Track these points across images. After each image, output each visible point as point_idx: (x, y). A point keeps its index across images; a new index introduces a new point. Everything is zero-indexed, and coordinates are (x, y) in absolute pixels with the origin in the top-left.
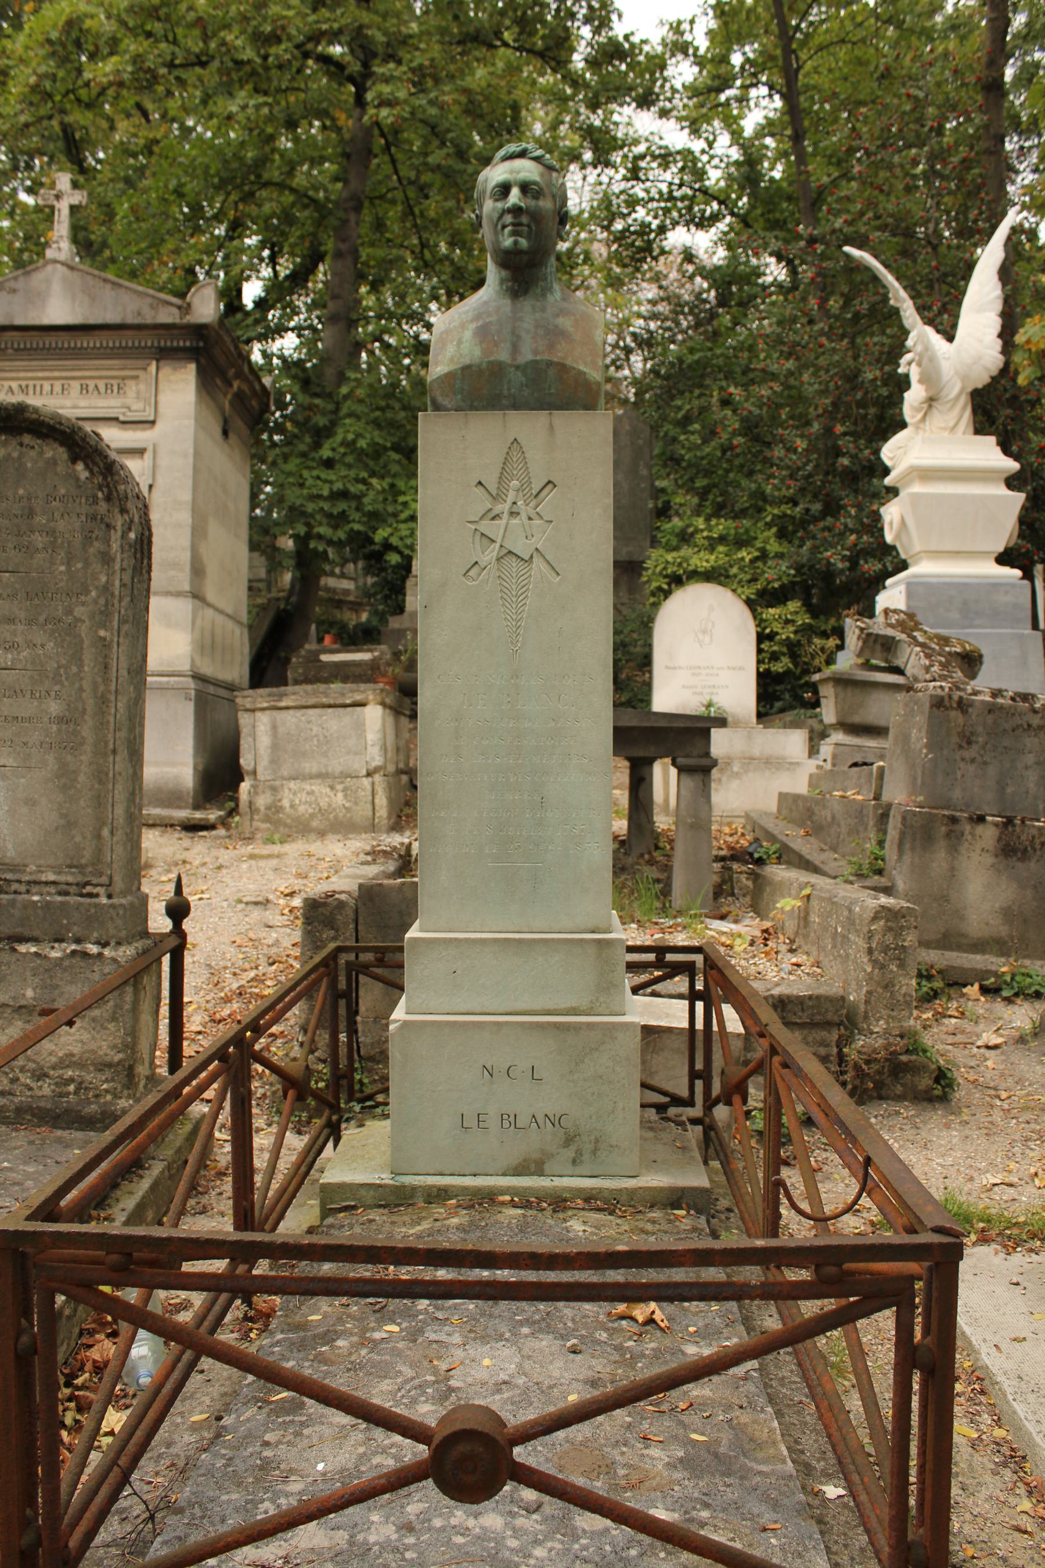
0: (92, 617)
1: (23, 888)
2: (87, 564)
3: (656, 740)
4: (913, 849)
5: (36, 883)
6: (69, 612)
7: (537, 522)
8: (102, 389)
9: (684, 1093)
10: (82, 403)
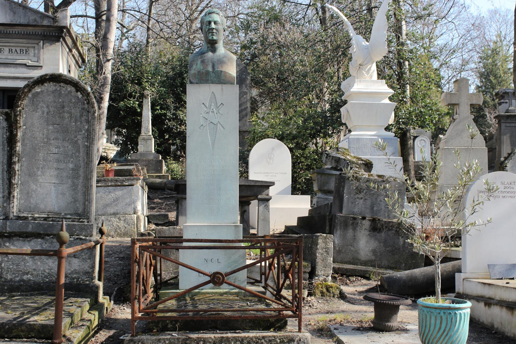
0: (83, 138)
2: (81, 122)
3: (252, 193)
4: (340, 229)
6: (76, 137)
7: (219, 114)
8: (19, 52)
9: (259, 279)
10: (10, 57)
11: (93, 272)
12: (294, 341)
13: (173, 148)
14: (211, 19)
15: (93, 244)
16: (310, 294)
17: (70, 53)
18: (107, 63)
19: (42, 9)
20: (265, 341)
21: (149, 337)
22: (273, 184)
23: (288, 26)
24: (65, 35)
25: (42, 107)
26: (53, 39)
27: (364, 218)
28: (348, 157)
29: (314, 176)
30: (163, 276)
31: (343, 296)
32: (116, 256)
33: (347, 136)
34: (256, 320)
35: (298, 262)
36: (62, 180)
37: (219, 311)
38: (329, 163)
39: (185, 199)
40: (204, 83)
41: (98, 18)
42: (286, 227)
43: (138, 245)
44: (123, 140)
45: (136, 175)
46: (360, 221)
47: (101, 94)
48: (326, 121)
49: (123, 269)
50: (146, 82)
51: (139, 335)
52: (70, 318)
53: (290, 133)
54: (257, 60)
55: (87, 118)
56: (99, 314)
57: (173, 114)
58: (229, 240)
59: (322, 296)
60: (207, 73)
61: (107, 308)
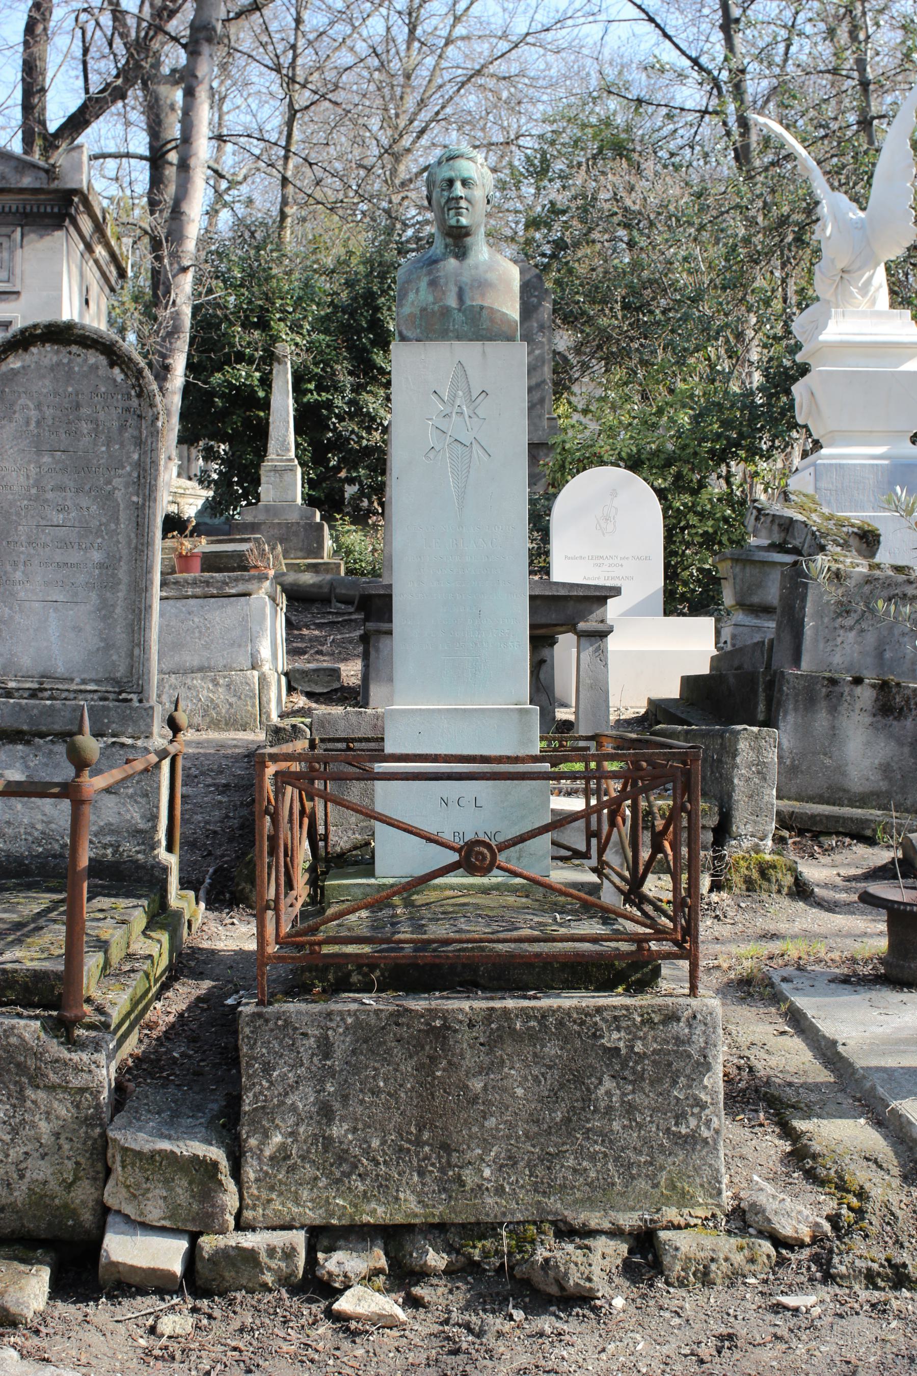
0: (127, 486)
1: (72, 696)
2: (122, 445)
3: (564, 615)
4: (796, 710)
5: (81, 691)
6: (109, 482)
7: (475, 419)
9: (582, 847)
11: (154, 829)
12: (678, 1020)
13: (350, 490)
14: (453, 174)
15: (153, 758)
16: (716, 886)
17: (87, 255)
18: (181, 277)
19: (17, 147)
20: (603, 1019)
21: (303, 1006)
22: (616, 591)
23: (649, 166)
24: (77, 209)
25: (25, 407)
26: (47, 221)
27: (858, 681)
28: (814, 517)
29: (725, 568)
30: (333, 839)
31: (805, 891)
32: (209, 781)
33: (811, 458)
34: (579, 964)
35: (689, 814)
36: (76, 594)
37: (481, 941)
38: (764, 533)
39: (390, 633)
40: (436, 340)
41: (156, 159)
42: (651, 702)
43: (271, 769)
44: (220, 473)
45: (256, 567)
46: (847, 689)
47: (164, 356)
48: (753, 418)
49: (227, 817)
50: (280, 320)
51: (278, 1001)
52: (101, 955)
53: (658, 450)
54: (567, 256)
55: (136, 433)
56: (172, 939)
57: (351, 403)
58: (508, 758)
59: (748, 890)
60: (446, 312)
61: (189, 922)
